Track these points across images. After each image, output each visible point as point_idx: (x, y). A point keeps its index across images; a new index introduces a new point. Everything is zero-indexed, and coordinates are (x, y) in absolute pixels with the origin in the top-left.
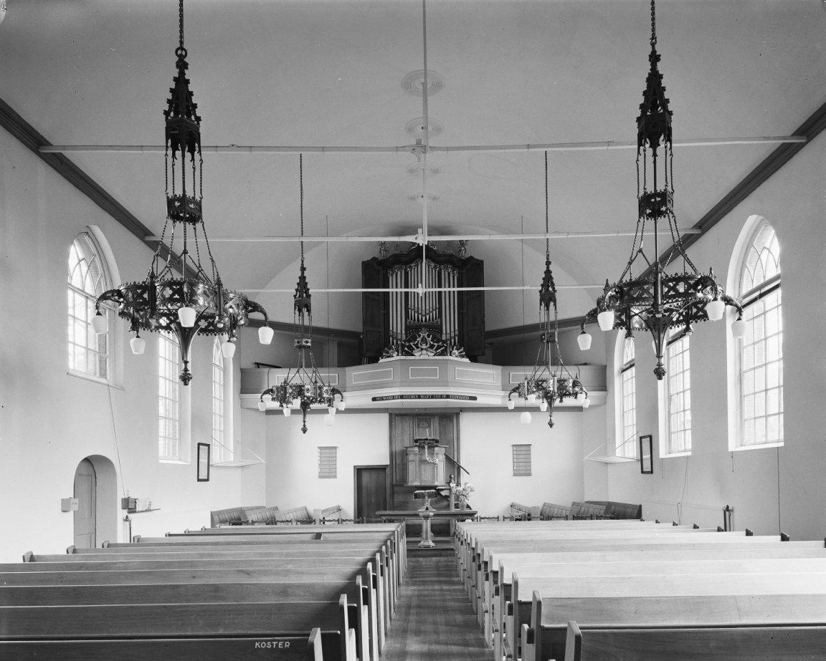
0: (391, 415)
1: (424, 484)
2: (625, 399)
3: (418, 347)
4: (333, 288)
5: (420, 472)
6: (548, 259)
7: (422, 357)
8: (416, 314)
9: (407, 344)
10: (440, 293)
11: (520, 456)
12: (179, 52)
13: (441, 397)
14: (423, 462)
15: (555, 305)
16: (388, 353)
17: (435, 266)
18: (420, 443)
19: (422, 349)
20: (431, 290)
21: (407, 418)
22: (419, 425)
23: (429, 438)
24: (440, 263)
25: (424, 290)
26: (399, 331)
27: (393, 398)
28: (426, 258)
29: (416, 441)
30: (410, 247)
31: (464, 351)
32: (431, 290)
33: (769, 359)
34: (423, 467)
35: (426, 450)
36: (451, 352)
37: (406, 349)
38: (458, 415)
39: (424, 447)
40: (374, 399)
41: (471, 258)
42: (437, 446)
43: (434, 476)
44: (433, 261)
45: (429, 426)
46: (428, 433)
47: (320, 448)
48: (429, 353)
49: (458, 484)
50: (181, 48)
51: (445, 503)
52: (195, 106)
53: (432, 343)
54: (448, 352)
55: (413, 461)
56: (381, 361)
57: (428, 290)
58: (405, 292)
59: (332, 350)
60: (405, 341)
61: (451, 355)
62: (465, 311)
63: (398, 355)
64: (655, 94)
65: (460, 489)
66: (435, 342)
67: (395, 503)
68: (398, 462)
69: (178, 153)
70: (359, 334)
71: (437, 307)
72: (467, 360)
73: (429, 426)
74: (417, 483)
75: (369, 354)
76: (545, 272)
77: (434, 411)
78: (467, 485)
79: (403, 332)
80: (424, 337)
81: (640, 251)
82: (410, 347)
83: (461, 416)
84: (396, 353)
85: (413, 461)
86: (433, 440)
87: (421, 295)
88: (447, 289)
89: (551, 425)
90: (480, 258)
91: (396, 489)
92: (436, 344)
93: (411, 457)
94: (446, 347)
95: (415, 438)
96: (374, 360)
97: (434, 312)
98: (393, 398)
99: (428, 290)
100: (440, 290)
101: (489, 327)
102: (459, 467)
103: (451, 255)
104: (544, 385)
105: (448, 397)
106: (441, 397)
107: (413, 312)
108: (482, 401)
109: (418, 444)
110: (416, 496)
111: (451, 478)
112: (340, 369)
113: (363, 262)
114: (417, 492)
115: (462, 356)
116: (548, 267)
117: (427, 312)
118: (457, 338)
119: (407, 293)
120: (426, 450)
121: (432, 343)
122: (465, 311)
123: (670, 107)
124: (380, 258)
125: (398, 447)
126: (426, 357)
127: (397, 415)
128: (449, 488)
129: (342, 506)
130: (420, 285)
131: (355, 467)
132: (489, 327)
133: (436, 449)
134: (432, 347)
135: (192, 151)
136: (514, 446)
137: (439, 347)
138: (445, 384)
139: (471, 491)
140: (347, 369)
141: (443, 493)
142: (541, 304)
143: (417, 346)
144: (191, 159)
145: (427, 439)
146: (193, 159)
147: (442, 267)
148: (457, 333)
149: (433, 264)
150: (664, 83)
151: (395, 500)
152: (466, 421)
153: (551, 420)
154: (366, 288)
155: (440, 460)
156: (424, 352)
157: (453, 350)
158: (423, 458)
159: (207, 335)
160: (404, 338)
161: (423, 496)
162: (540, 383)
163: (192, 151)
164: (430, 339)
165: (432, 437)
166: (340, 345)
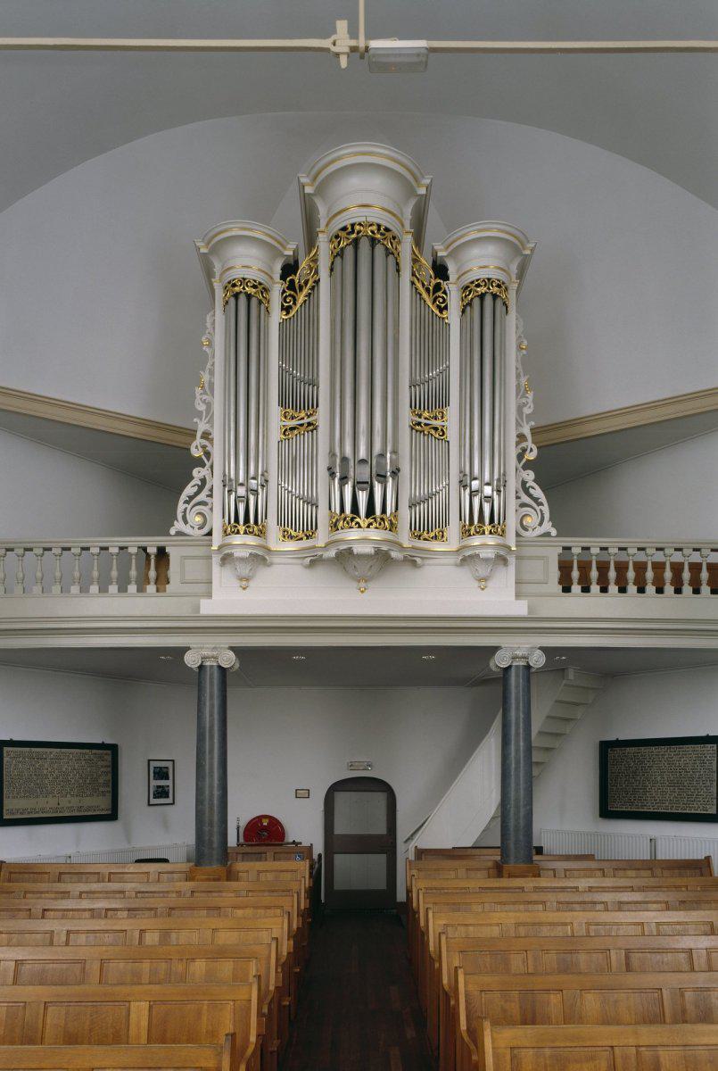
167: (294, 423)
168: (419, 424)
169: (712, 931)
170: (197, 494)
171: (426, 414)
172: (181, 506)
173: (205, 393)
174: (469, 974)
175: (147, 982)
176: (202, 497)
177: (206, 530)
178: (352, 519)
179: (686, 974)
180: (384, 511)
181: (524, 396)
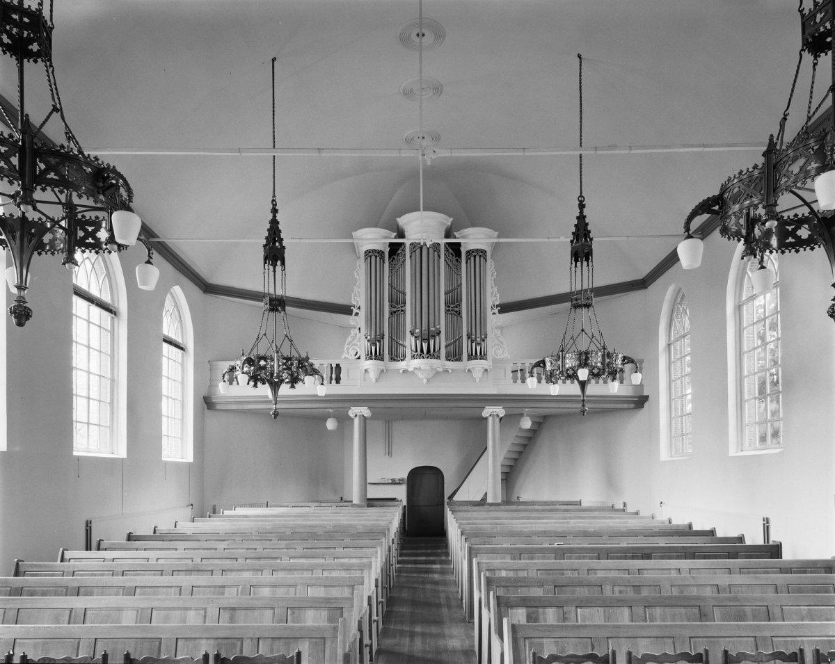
2: (673, 366)
12: (580, 199)
33: (91, 426)
50: (581, 196)
52: (589, 232)
64: (275, 234)
69: (579, 264)
81: (265, 335)
123: (284, 243)
135: (587, 260)
146: (588, 265)
150: (280, 227)
163: (587, 260)
167: (395, 309)
168: (449, 310)
169: (347, 657)
170: (353, 340)
171: (452, 306)
172: (346, 346)
173: (356, 296)
174: (274, 145)
175: (299, 587)
176: (355, 342)
177: (357, 356)
178: (420, 355)
179: (128, 606)
180: (434, 351)
181: (495, 296)
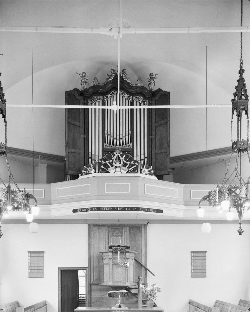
0: (89, 225)
1: (116, 284)
3: (112, 166)
4: (38, 104)
5: (113, 274)
6: (241, 67)
7: (116, 174)
8: (112, 139)
9: (103, 162)
10: (132, 110)
11: (197, 261)
13: (132, 209)
14: (115, 264)
15: (247, 113)
16: (86, 170)
17: (128, 97)
18: (113, 249)
19: (116, 167)
20: (124, 107)
21: (103, 228)
22: (112, 234)
23: (121, 245)
24: (133, 95)
25: (119, 107)
26: (97, 153)
27: (91, 209)
28: (120, 90)
29: (110, 247)
30: (107, 80)
31: (152, 169)
32: (124, 107)
34: (116, 269)
35: (119, 255)
36: (141, 170)
37: (102, 167)
38: (145, 225)
39: (117, 253)
40: (75, 211)
41: (159, 90)
42: (128, 252)
43: (126, 278)
44: (128, 93)
45: (122, 235)
46: (120, 241)
47: (29, 252)
48: (122, 171)
49: (145, 284)
51: (135, 299)
53: (125, 162)
54: (139, 170)
55: (107, 264)
56: (81, 177)
57: (122, 107)
58: (102, 109)
59: (42, 171)
60: (101, 160)
61: (141, 173)
62: (153, 137)
63: (95, 172)
65: (149, 289)
66: (128, 161)
67: (93, 298)
68: (95, 264)
70: (63, 158)
71: (130, 133)
72: (155, 178)
73: (122, 235)
74: (110, 284)
75: (71, 172)
76: (238, 81)
77: (127, 223)
78: (155, 286)
79: (101, 154)
80: (118, 156)
82: (105, 165)
83: (148, 227)
84: (94, 170)
85: (107, 264)
86: (125, 246)
87: (115, 112)
88: (138, 107)
89: (240, 233)
90: (169, 91)
91: (93, 287)
92: (128, 163)
93: (106, 261)
94: (137, 166)
95: (110, 245)
96: (75, 177)
97: (127, 137)
98: (91, 209)
99: (122, 107)
100: (132, 107)
101: (173, 154)
102: (146, 269)
103: (143, 88)
104: (238, 191)
105: (138, 209)
106: (132, 209)
107: (109, 137)
108: (168, 213)
109: (111, 250)
110: (110, 295)
111: (139, 279)
112: (48, 185)
113: (66, 92)
114: (111, 292)
115: (151, 174)
116: (241, 76)
117: (121, 137)
118: (146, 160)
119: (104, 110)
120: (119, 255)
121: (125, 162)
122: (153, 137)
124: (80, 88)
125: (96, 252)
126: (120, 174)
127: (94, 225)
128: (137, 287)
129: (49, 301)
130: (115, 102)
131: (59, 268)
132: (173, 154)
133: (127, 254)
134: (125, 165)
136: (192, 252)
137: (131, 166)
138: (135, 197)
139: (157, 291)
140: (53, 185)
141: (133, 291)
142: (233, 114)
143: (112, 164)
144: (4, 121)
145: (119, 246)
147: (134, 98)
148: (146, 156)
149: (126, 96)
151: (93, 296)
152: (152, 230)
153: (240, 228)
154: (68, 104)
155: (130, 264)
156: (118, 169)
157: (143, 168)
158: (116, 262)
159: (18, 210)
160: (101, 157)
161: (116, 295)
162: (233, 190)
164: (123, 158)
165: (124, 244)
166: (49, 167)
